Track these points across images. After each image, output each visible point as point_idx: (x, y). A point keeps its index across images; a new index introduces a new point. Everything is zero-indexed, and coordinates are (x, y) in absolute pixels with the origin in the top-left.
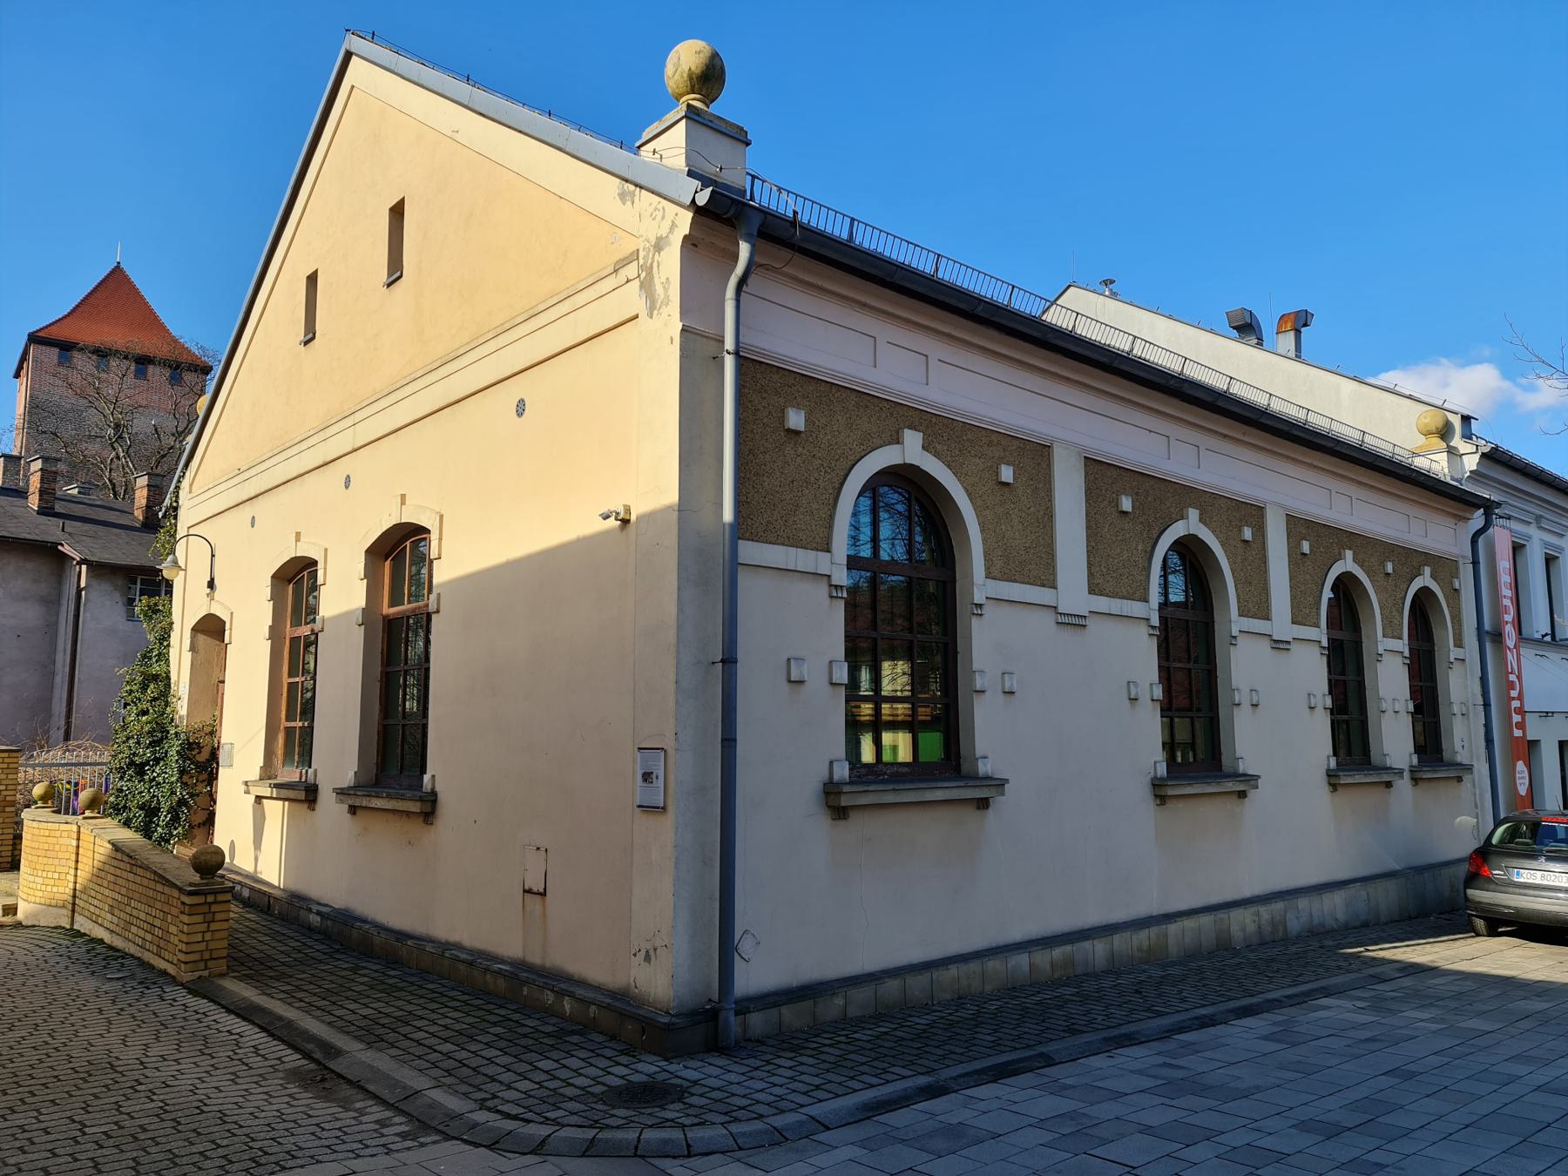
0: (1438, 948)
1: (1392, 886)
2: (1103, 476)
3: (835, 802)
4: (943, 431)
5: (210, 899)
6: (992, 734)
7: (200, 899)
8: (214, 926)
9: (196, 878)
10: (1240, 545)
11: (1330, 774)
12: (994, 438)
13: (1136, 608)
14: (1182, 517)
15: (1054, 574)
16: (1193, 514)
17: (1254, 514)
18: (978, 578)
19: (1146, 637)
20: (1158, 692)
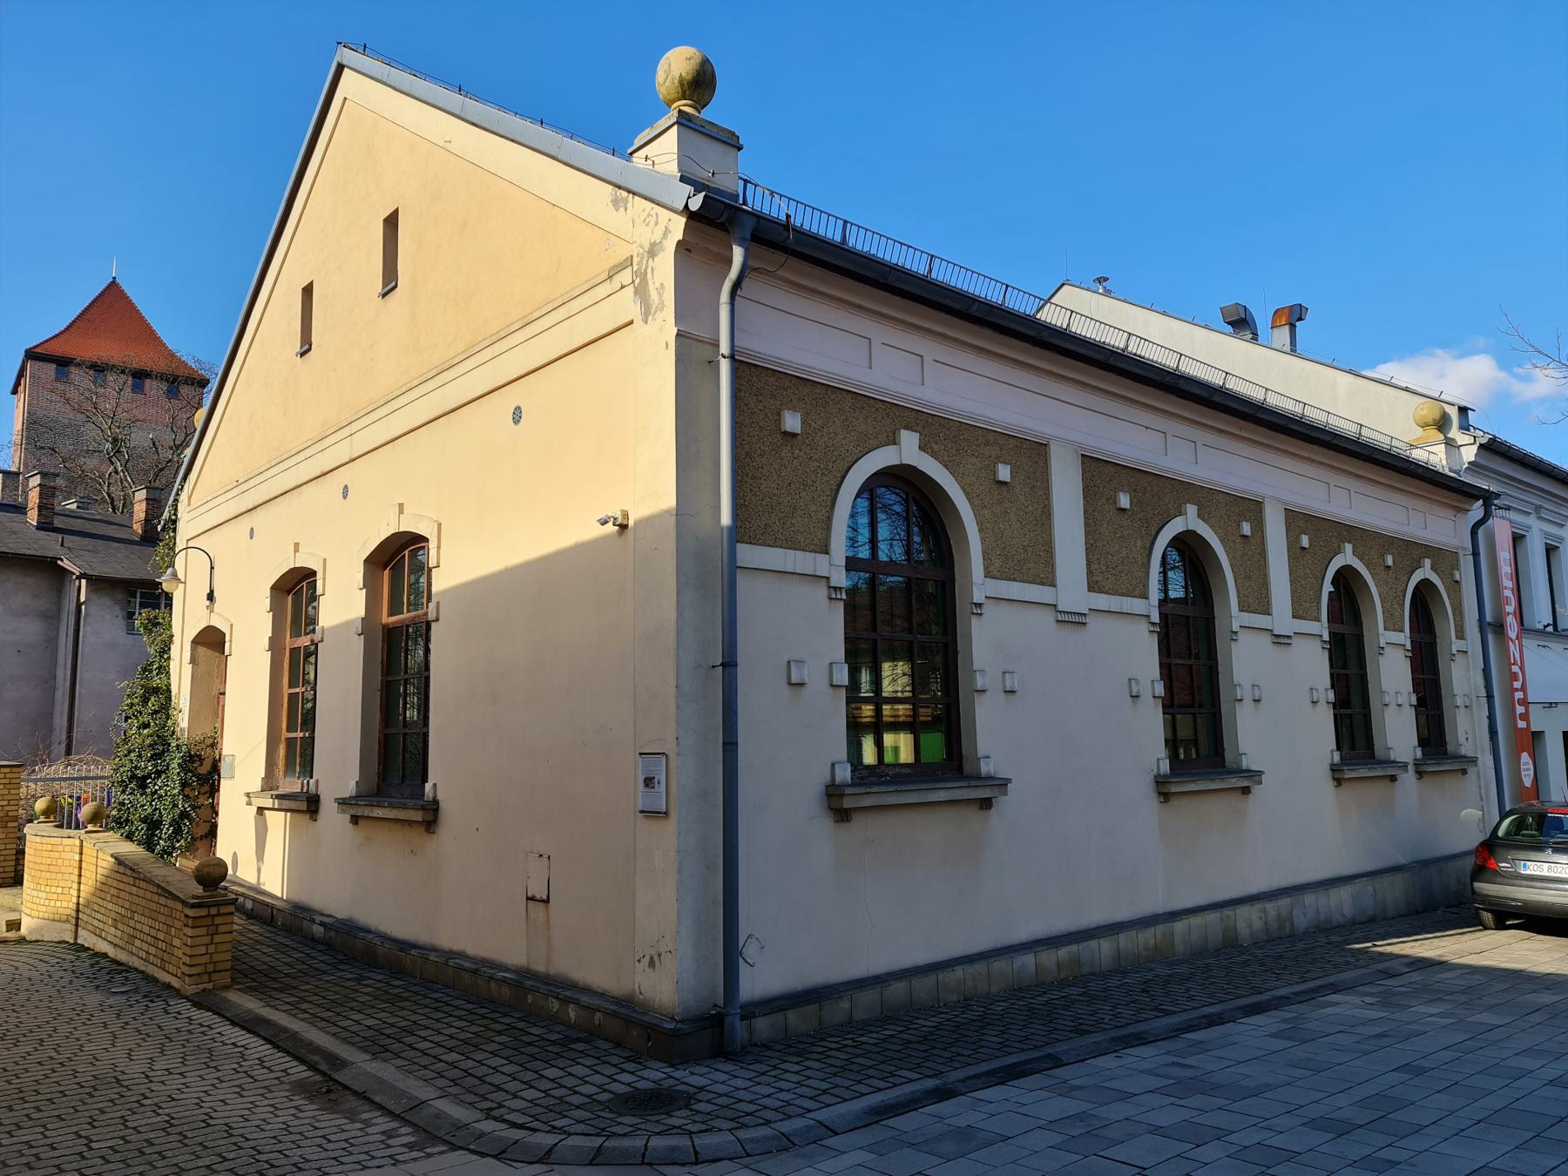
2: (1100, 474)
4: (940, 431)
6: (993, 734)
10: (1239, 540)
11: (1334, 769)
12: (991, 438)
16: (1191, 510)
17: (1032, 454)
18: (977, 578)
20: (1160, 689)
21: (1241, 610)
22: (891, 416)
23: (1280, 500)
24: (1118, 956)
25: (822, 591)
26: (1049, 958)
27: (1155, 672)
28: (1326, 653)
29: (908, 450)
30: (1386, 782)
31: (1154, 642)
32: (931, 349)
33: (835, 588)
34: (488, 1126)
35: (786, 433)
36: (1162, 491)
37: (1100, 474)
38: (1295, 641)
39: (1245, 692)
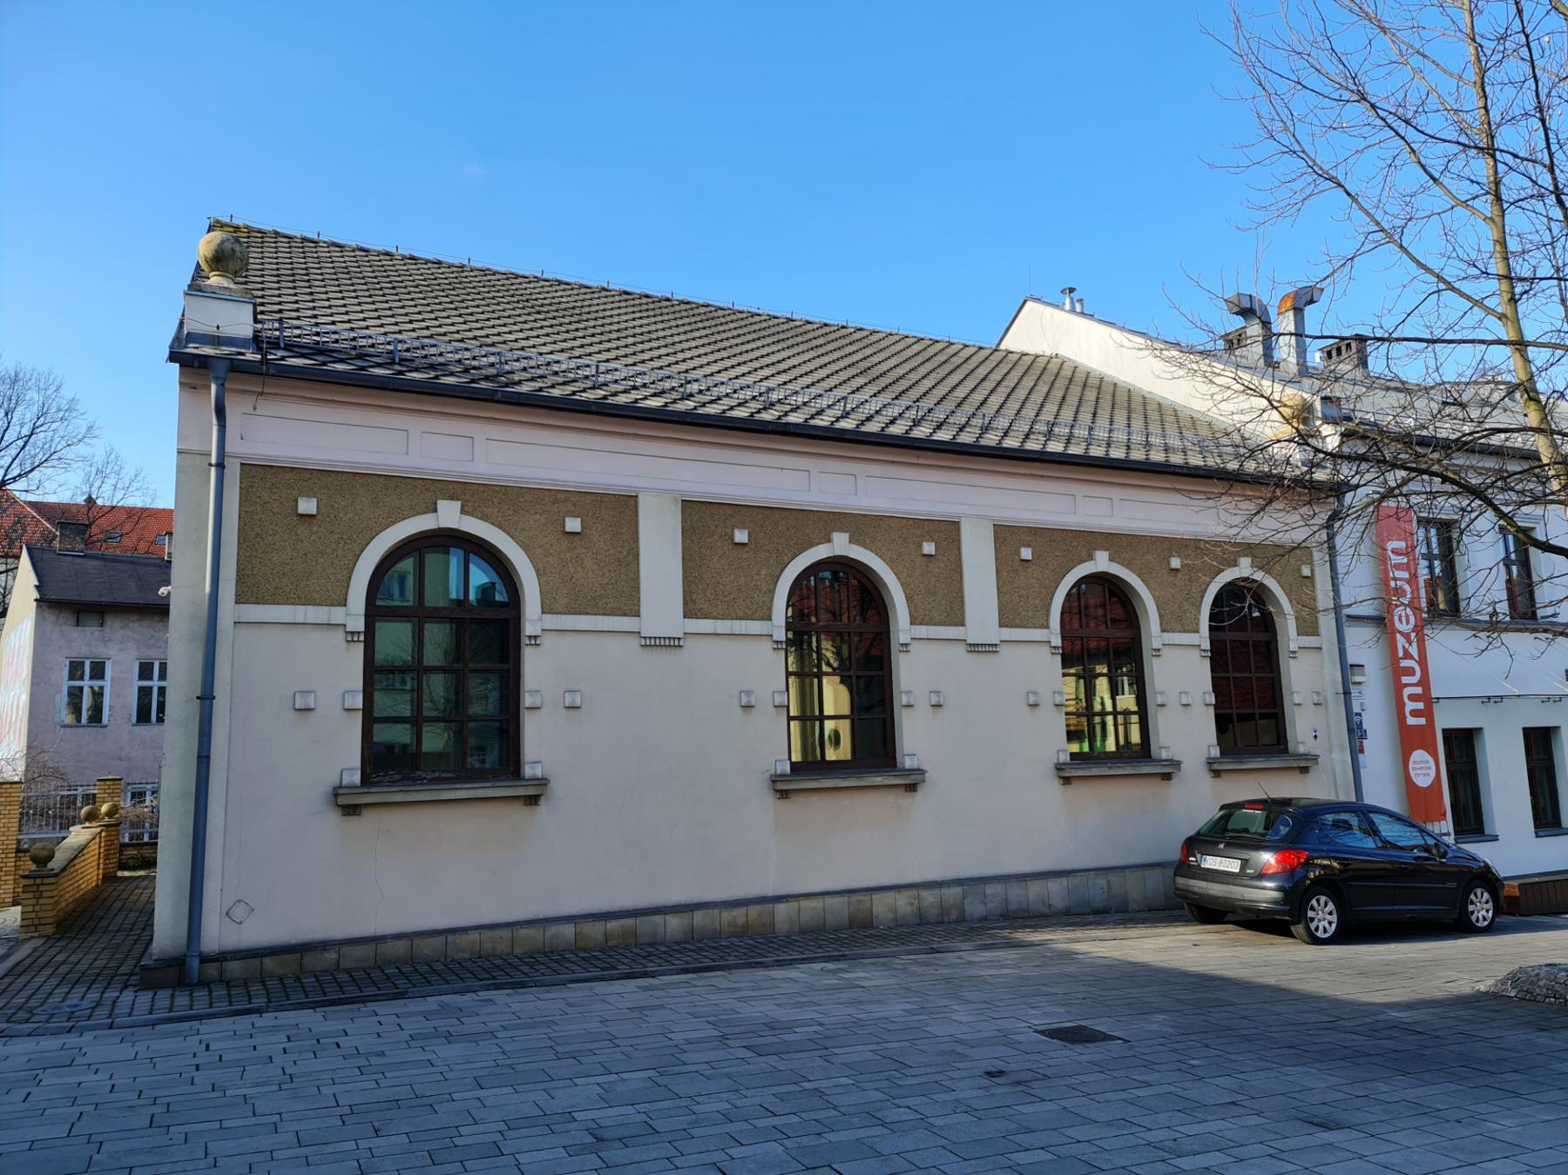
0: (1161, 942)
1: (1157, 873)
2: (701, 518)
3: (782, 788)
4: (861, 526)
5: (38, 881)
6: (915, 736)
7: (31, 882)
8: (42, 901)
9: (34, 867)
10: (919, 560)
11: (1210, 762)
12: (562, 497)
13: (755, 627)
14: (1090, 557)
15: (963, 614)
16: (1245, 562)
17: (948, 532)
18: (902, 626)
19: (770, 652)
20: (1212, 699)
21: (1163, 630)
22: (1090, 540)
23: (985, 517)
24: (607, 936)
25: (340, 636)
26: (739, 914)
27: (1208, 684)
28: (1208, 662)
29: (1102, 562)
30: (1157, 782)
31: (1206, 666)
32: (1117, 493)
33: (352, 633)
34: (1326, 862)
35: (301, 515)
36: (786, 525)
37: (701, 518)
38: (1003, 649)
39: (922, 700)
